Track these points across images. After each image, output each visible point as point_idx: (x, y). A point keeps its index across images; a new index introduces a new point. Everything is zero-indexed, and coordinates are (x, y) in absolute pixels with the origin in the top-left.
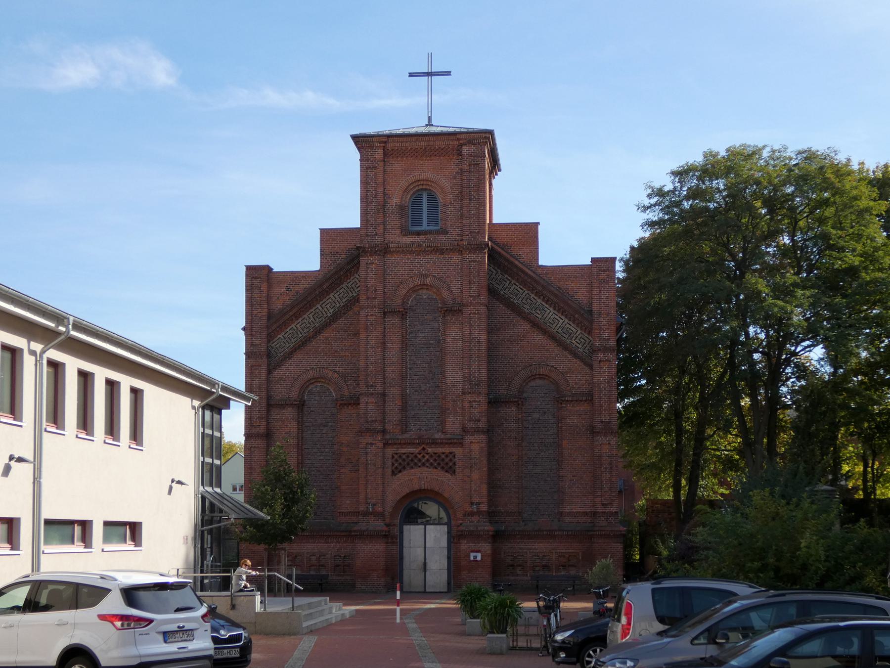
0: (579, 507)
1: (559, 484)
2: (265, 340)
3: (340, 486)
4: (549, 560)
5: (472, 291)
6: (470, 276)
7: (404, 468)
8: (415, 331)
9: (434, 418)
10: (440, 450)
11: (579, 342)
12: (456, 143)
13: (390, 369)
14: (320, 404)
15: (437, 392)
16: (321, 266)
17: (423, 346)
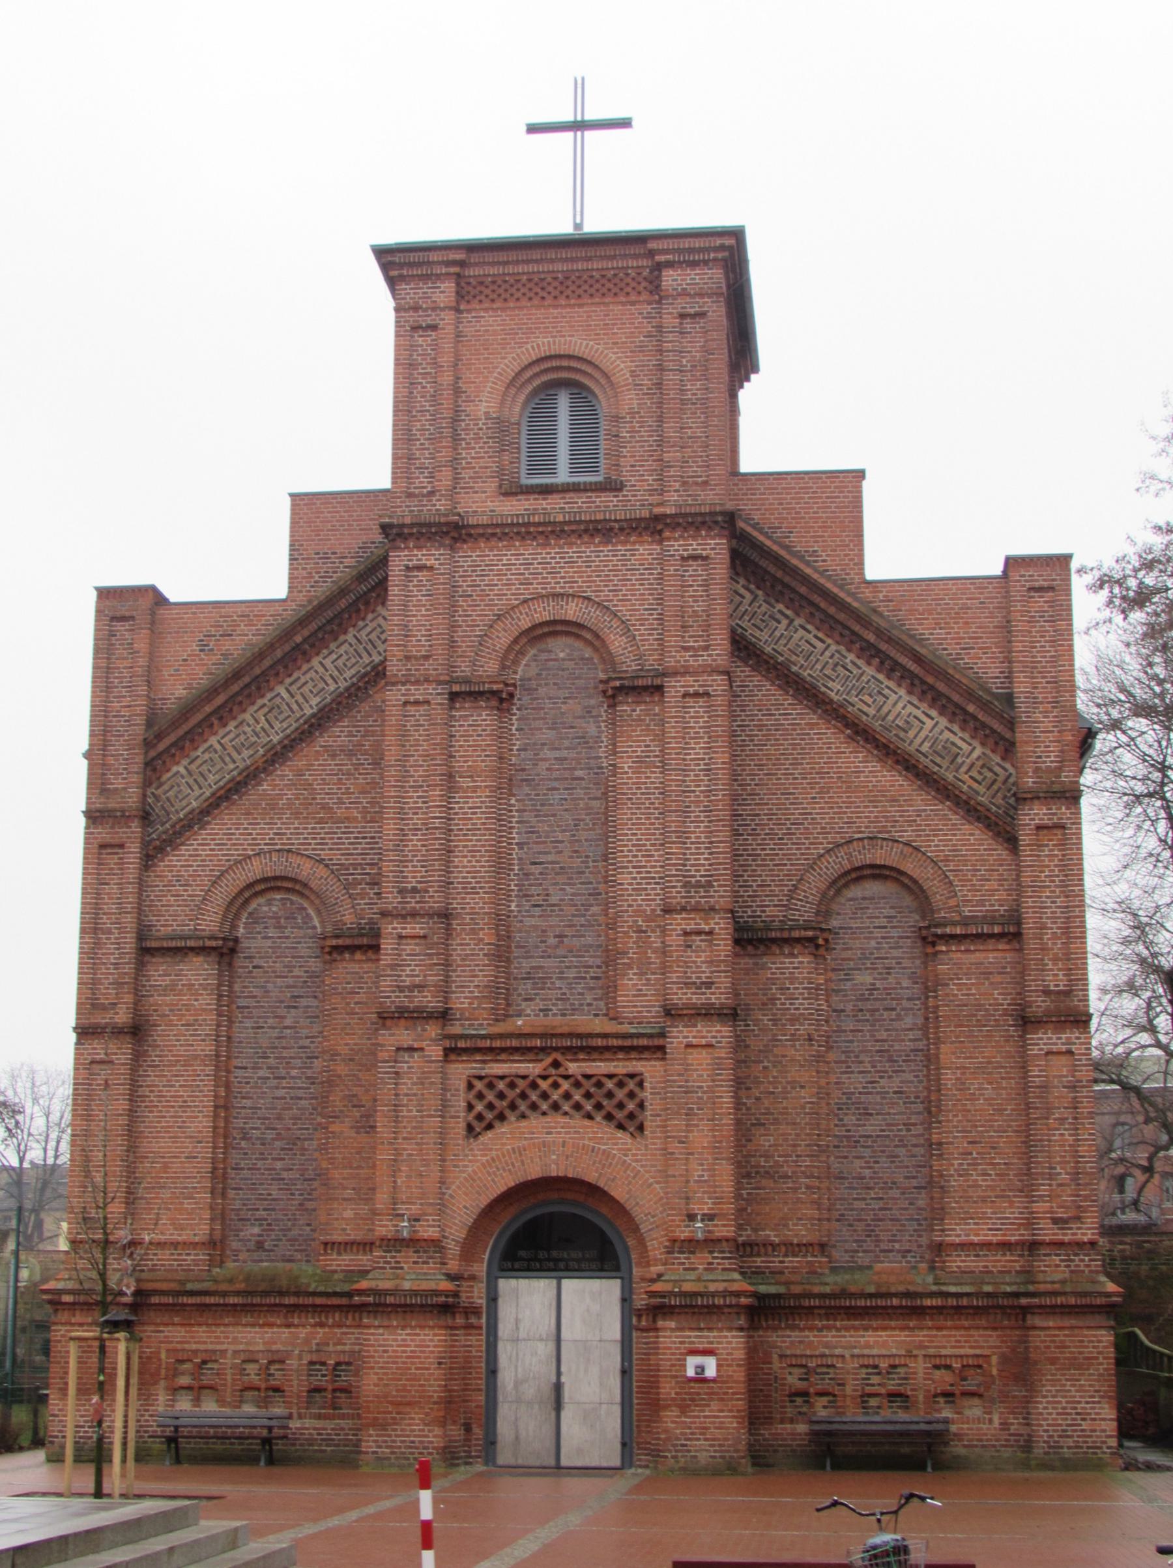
0: (990, 1229)
1: (931, 1167)
2: (135, 778)
3: (328, 1169)
4: (905, 1379)
5: (691, 637)
6: (683, 597)
7: (501, 1117)
8: (535, 744)
9: (585, 978)
10: (600, 1067)
11: (979, 778)
12: (645, 262)
13: (464, 846)
14: (280, 947)
15: (595, 909)
16: (291, 588)
17: (556, 784)
